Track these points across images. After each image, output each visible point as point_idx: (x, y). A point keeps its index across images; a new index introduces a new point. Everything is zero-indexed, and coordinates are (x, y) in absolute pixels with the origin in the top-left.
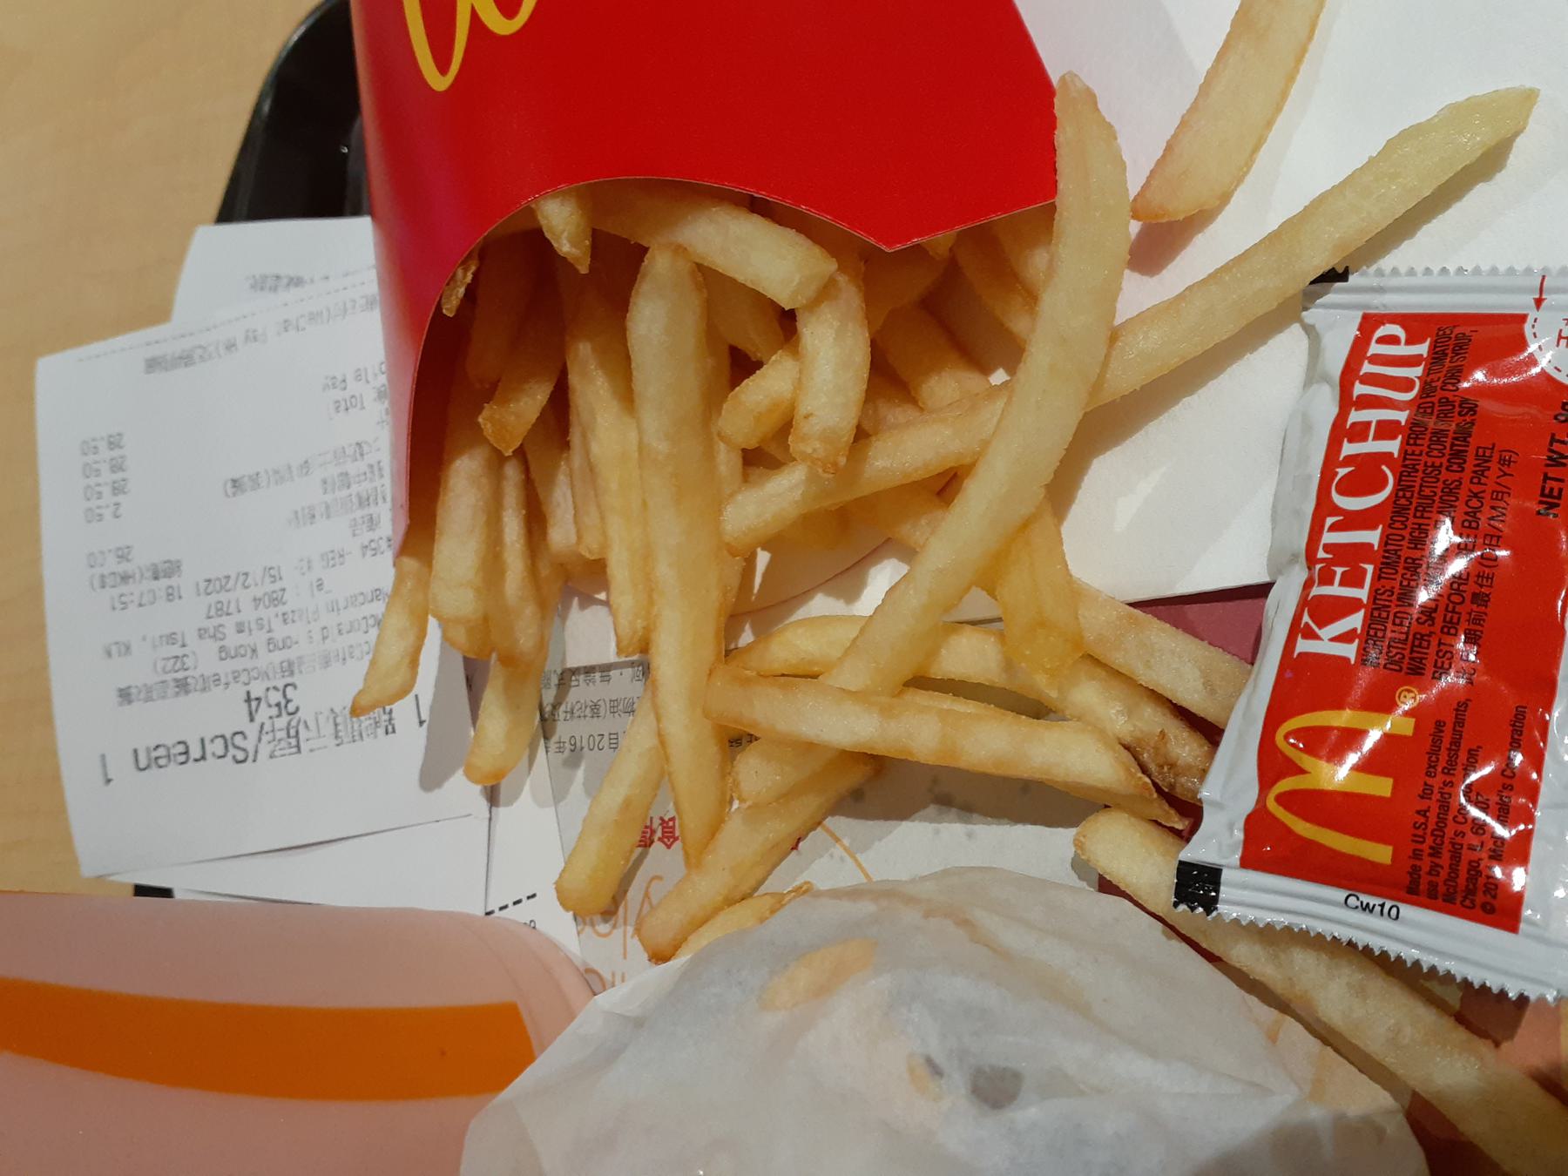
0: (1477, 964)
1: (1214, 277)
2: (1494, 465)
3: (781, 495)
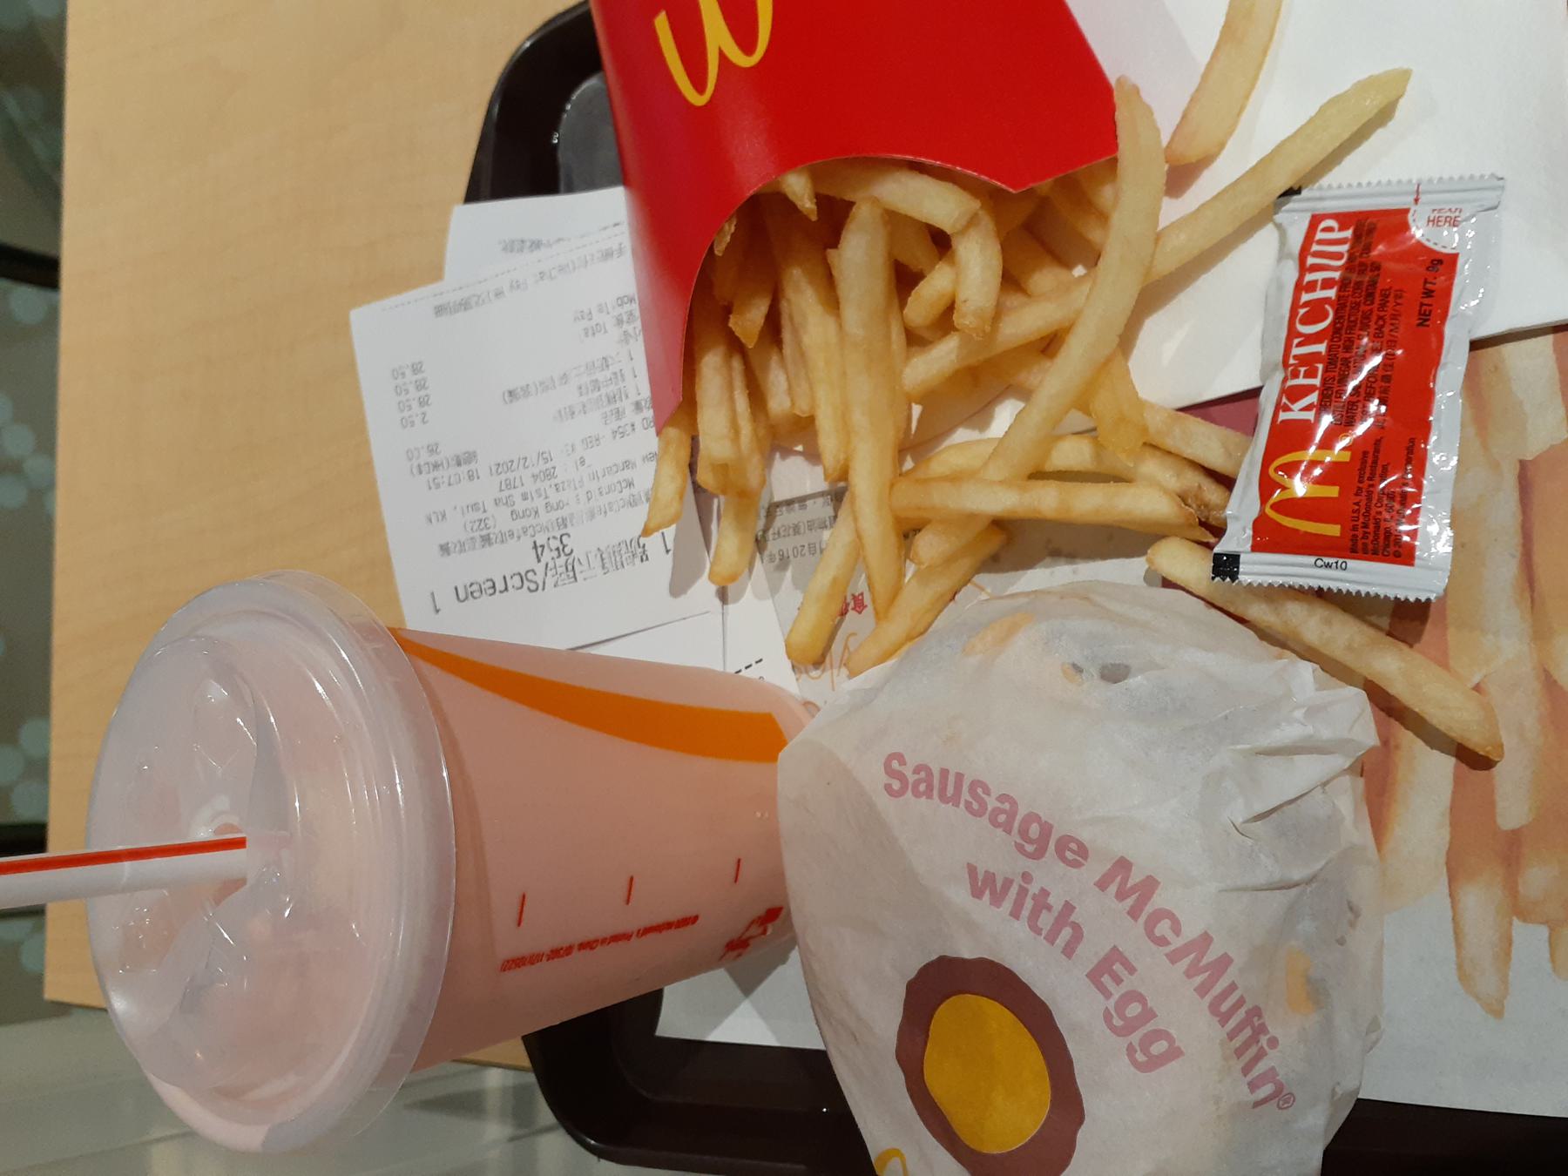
0: (1393, 587)
1: (1215, 198)
2: (1391, 299)
3: (943, 356)
